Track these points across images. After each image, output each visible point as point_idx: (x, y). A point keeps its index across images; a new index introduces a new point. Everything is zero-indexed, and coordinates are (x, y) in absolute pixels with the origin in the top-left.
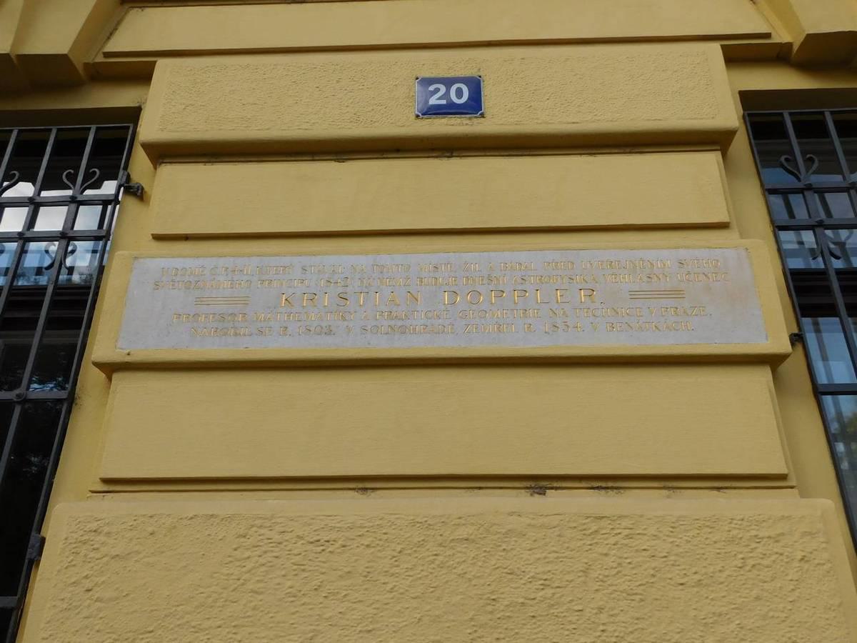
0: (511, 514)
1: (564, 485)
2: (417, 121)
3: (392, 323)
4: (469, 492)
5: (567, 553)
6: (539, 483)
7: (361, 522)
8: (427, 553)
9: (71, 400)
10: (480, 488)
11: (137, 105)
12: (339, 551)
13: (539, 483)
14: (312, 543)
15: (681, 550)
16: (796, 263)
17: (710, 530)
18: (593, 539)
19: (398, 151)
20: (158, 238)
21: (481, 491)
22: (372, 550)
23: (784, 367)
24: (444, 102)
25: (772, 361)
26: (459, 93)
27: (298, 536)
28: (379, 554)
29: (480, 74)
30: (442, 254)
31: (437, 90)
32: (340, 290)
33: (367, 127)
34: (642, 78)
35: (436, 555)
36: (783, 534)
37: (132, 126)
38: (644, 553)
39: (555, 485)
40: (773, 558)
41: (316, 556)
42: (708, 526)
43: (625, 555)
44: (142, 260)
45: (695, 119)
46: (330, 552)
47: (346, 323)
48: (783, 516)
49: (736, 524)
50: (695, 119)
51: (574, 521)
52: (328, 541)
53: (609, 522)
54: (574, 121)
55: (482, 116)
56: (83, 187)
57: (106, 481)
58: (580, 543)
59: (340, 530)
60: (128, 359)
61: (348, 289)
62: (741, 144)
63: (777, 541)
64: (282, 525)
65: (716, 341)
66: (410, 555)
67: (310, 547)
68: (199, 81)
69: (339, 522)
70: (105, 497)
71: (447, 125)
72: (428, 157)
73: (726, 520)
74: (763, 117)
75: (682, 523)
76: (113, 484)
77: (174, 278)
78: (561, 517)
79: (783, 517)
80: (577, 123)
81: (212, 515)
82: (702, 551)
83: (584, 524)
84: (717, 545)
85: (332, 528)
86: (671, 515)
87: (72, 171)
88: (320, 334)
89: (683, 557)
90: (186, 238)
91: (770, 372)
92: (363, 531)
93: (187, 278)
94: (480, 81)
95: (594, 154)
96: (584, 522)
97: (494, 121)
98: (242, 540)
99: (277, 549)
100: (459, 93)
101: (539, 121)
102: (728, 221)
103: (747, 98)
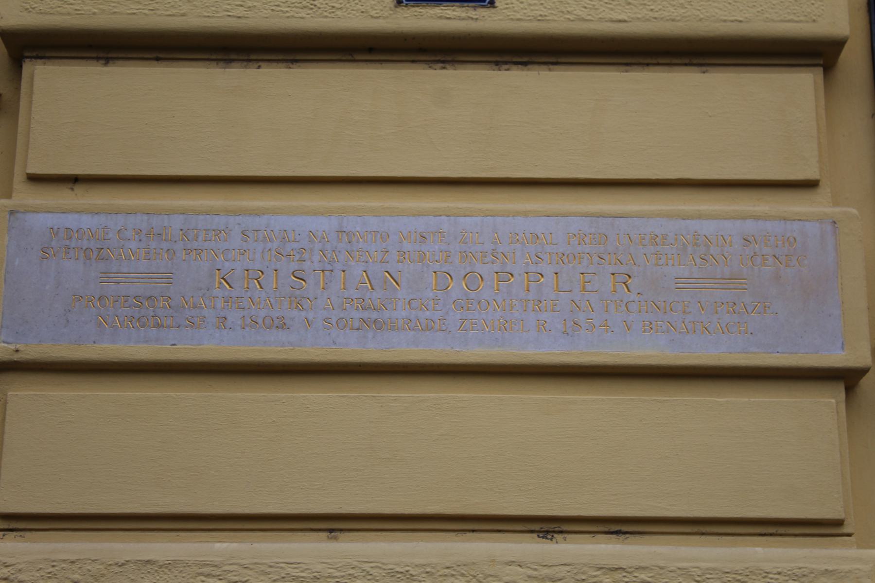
0: (510, 563)
1: (625, 528)
3: (365, 315)
4: (461, 536)
6: (548, 526)
7: (330, 571)
10: (473, 531)
13: (548, 526)
19: (371, 50)
20: (35, 179)
21: (475, 534)
30: (431, 217)
32: (294, 266)
33: (326, 17)
39: (625, 528)
44: (19, 215)
45: (789, 21)
47: (303, 314)
48: (826, 570)
49: (772, 579)
50: (789, 21)
51: (583, 573)
53: (625, 574)
54: (620, 17)
60: (16, 357)
61: (307, 265)
62: (855, 59)
64: (234, 573)
65: (779, 350)
69: (302, 572)
70: (6, 537)
71: (441, 17)
73: (760, 574)
75: (709, 576)
78: (568, 568)
80: (625, 21)
83: (595, 576)
86: (697, 567)
90: (74, 180)
91: (843, 390)
93: (85, 244)
95: (648, 65)
96: (595, 573)
101: (571, 17)
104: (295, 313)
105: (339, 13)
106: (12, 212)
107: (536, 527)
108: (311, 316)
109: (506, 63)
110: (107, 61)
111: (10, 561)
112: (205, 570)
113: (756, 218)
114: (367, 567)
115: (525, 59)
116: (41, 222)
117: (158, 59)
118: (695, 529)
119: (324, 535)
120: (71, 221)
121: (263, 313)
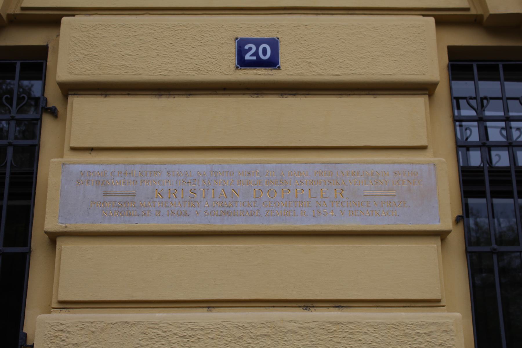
1: (342, 305)
2: (237, 71)
3: (223, 209)
4: (268, 309)
5: (319, 342)
6: (308, 304)
8: (245, 342)
9: (30, 252)
11: (45, 44)
12: (197, 341)
13: (308, 304)
14: (182, 337)
15: (379, 340)
16: (475, 159)
17: (395, 330)
18: (333, 334)
19: (225, 89)
21: (274, 308)
22: (215, 341)
23: (450, 237)
24: (254, 58)
25: (442, 235)
26: (265, 52)
27: (174, 333)
28: (219, 343)
29: (278, 36)
31: (250, 49)
32: (191, 187)
34: (382, 43)
35: (249, 343)
36: (432, 332)
37: (44, 62)
38: (359, 342)
39: (342, 305)
40: (426, 344)
41: (185, 344)
42: (394, 328)
43: (350, 343)
44: (67, 166)
45: (413, 74)
46: (192, 342)
47: (195, 209)
50: (413, 74)
51: (324, 325)
52: (190, 336)
54: (337, 73)
55: (279, 67)
56: (19, 107)
57: (61, 302)
58: (325, 337)
59: (196, 330)
60: (66, 230)
61: (197, 187)
62: (442, 92)
63: (429, 335)
66: (235, 343)
67: (180, 339)
68: (91, 36)
71: (256, 74)
72: (244, 94)
74: (460, 63)
76: (66, 305)
77: (88, 178)
78: (316, 323)
79: (433, 323)
80: (339, 75)
81: (126, 322)
82: (390, 341)
84: (398, 338)
85: (193, 329)
87: (9, 96)
88: (180, 215)
89: (379, 344)
90: (92, 149)
92: (209, 331)
94: (278, 41)
95: (350, 94)
97: (288, 71)
98: (144, 335)
99: (163, 340)
100: (265, 52)
101: (315, 73)
102: (427, 145)
103: (452, 51)
104: (191, 208)
105: (210, 73)
106: (63, 164)
107: (302, 305)
108: (198, 210)
109: (286, 94)
110: (106, 95)
111: (64, 322)
112: (152, 326)
113: (400, 163)
114: (225, 324)
115: (294, 93)
116: (77, 168)
117: (129, 94)
118: (374, 304)
119: (206, 309)
120: (90, 168)
121: (177, 209)
